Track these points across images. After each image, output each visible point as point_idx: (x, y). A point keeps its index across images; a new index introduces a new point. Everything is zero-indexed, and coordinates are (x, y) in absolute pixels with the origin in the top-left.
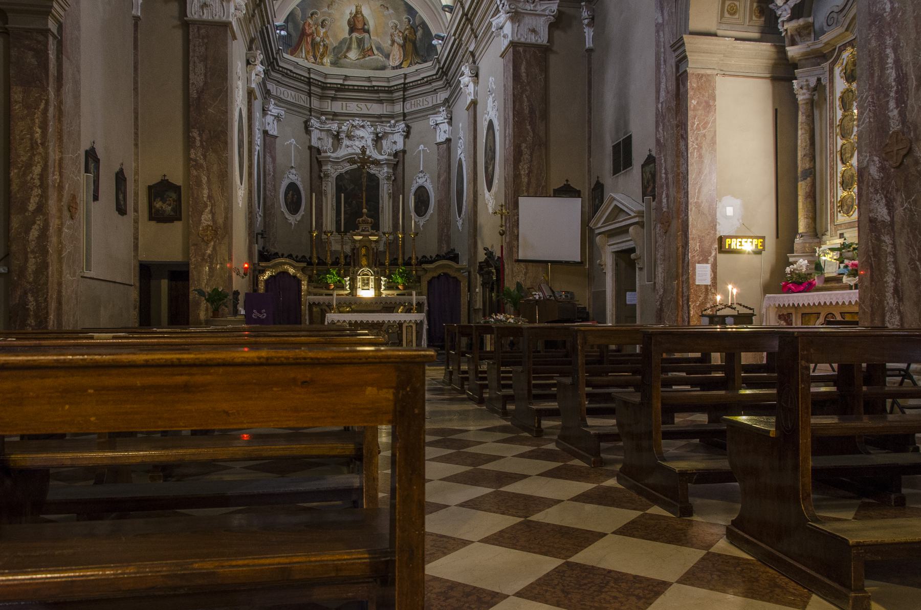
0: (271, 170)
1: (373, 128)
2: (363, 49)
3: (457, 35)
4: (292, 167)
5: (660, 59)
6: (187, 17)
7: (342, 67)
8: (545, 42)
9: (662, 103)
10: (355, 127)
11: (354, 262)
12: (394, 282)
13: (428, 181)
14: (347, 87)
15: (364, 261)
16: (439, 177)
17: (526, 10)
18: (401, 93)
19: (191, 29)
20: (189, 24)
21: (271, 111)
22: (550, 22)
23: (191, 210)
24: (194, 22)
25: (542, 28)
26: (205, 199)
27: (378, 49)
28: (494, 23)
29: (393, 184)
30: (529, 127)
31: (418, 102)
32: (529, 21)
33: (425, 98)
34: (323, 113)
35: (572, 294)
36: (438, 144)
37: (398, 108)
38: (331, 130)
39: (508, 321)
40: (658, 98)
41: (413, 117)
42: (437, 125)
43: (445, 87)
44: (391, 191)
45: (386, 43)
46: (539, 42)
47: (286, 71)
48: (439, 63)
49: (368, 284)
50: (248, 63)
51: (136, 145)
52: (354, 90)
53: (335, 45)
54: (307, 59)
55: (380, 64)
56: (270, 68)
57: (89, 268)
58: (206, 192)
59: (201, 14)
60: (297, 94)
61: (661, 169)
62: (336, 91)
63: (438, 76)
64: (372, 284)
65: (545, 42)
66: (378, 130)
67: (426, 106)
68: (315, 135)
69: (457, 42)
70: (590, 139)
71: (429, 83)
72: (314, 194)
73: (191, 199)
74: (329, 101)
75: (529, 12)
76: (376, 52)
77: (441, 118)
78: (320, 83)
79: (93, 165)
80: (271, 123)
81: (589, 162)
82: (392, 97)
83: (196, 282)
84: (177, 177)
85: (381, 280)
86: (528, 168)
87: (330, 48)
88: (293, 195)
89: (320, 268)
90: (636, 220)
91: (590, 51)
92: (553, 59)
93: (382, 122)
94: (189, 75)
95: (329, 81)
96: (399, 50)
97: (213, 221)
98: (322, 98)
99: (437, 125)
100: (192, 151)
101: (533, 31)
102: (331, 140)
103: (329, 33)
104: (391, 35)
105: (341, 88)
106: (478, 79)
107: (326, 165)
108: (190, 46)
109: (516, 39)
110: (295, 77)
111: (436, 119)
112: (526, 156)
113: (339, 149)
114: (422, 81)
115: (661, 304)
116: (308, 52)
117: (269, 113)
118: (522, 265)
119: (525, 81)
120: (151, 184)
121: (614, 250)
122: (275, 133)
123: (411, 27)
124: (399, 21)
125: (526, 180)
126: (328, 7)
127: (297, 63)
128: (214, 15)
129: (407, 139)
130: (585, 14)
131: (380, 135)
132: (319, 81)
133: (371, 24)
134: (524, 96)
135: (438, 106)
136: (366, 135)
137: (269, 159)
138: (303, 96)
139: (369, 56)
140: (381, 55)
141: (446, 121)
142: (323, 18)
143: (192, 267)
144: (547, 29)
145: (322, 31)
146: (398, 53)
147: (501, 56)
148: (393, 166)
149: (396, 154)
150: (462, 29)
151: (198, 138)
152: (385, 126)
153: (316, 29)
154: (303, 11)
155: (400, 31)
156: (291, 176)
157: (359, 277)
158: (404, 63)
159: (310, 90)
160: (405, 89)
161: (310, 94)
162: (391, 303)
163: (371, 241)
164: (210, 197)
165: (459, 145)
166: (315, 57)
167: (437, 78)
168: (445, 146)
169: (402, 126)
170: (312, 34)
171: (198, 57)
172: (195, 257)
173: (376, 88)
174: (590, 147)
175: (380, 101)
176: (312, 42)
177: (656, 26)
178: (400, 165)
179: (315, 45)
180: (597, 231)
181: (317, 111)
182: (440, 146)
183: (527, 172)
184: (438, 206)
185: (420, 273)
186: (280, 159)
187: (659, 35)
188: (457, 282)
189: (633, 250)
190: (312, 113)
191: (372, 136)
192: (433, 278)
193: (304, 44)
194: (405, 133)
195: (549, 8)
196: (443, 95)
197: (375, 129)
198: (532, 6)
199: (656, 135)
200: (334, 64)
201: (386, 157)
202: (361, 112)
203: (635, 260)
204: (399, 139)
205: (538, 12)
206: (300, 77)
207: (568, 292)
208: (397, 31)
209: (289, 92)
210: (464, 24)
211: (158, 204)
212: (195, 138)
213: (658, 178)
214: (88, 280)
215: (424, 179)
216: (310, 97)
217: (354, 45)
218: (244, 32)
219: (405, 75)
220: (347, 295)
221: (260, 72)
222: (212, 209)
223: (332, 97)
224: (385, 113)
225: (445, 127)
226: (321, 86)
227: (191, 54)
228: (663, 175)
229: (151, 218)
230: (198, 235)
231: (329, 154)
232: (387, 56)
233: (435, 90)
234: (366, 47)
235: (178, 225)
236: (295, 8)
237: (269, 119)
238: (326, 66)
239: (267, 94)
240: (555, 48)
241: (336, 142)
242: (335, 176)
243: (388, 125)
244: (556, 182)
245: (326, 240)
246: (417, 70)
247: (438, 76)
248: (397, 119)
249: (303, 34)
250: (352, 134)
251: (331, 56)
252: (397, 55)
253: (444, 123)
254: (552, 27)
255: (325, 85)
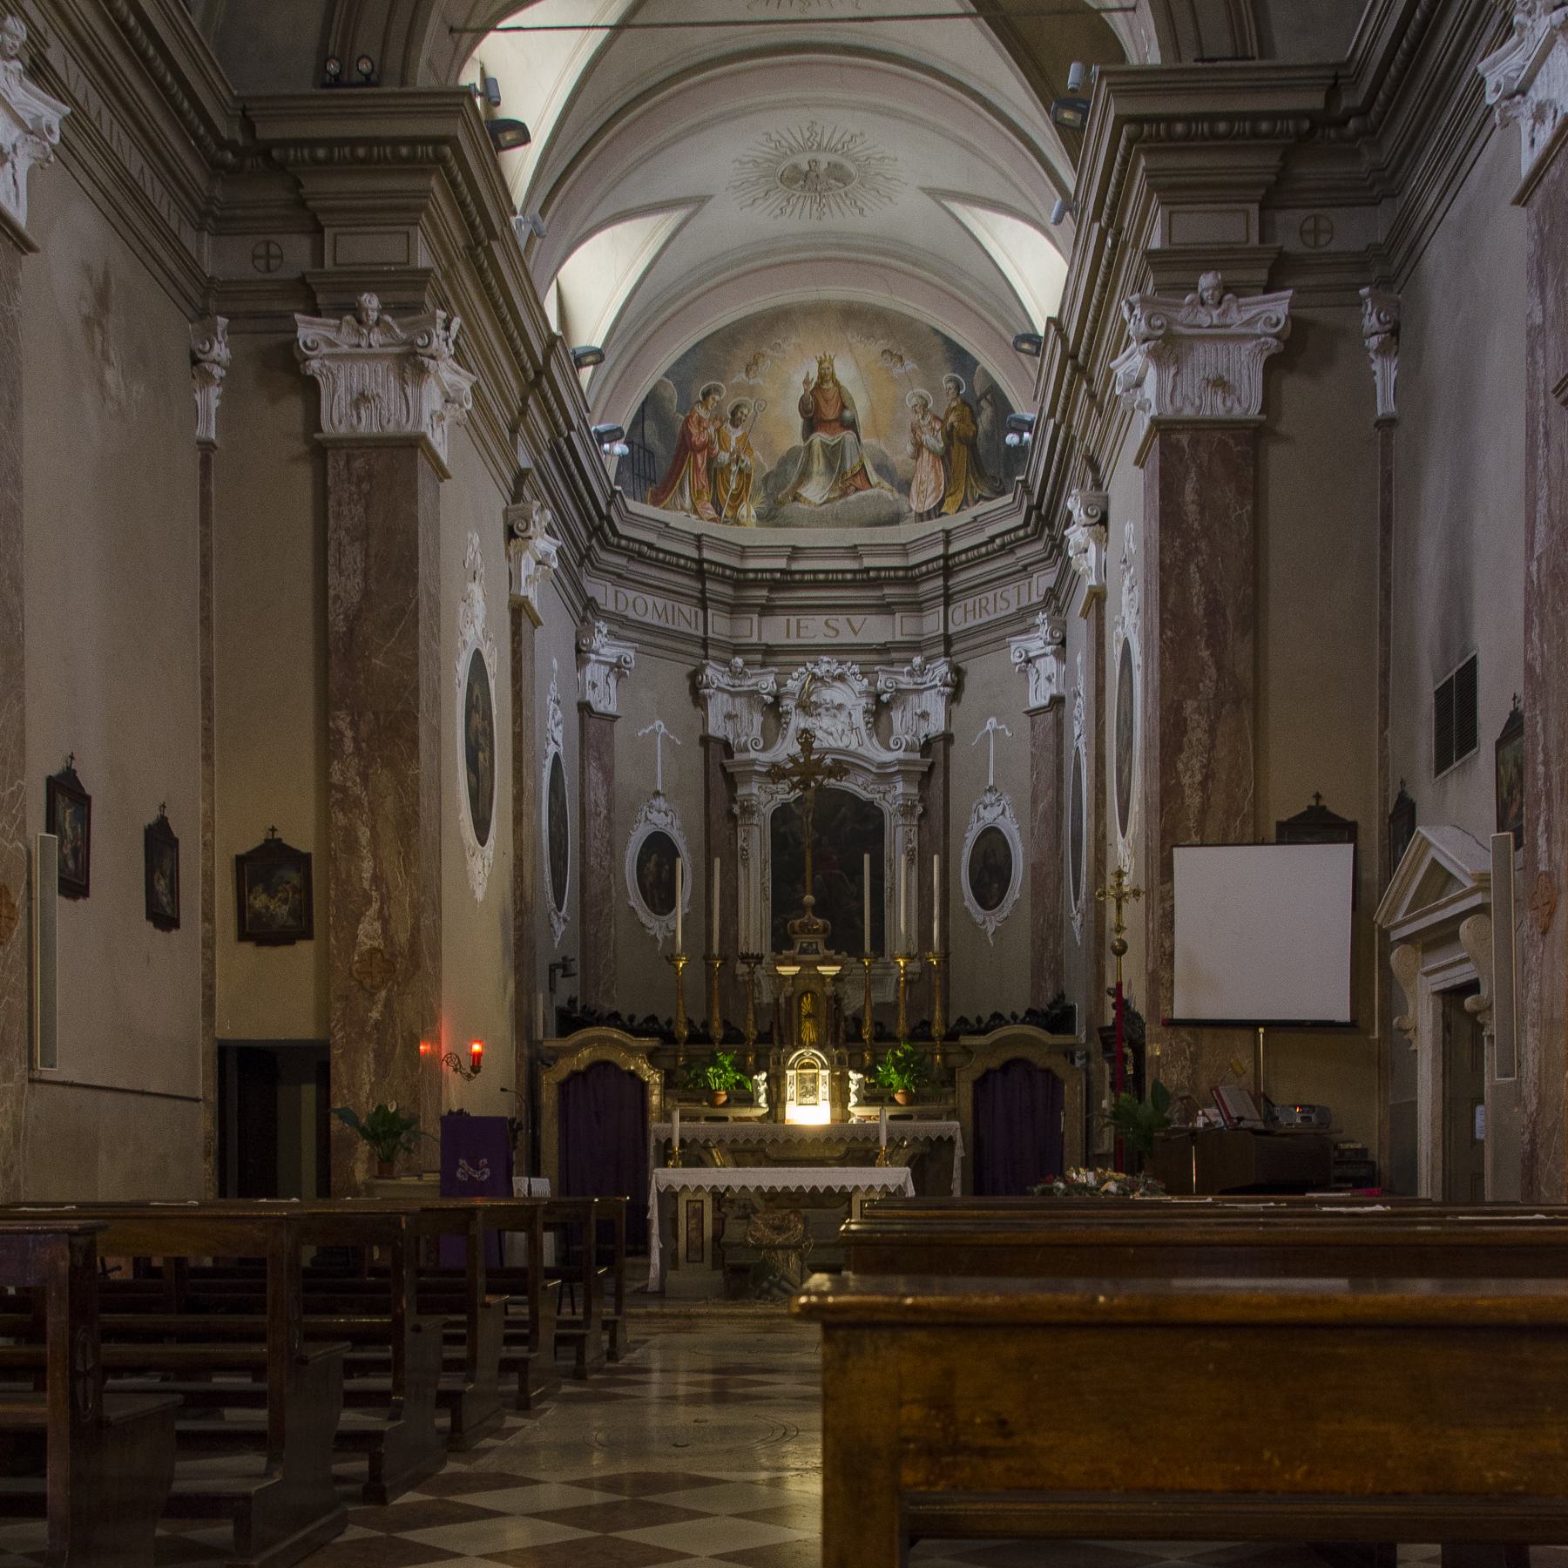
0: (602, 801)
1: (866, 681)
2: (842, 473)
3: (1058, 415)
4: (657, 794)
5: (1535, 431)
6: (320, 430)
7: (786, 526)
8: (1254, 411)
9: (1539, 559)
10: (821, 679)
11: (781, 1036)
12: (882, 1085)
13: (1007, 813)
14: (797, 577)
15: (809, 1031)
16: (1034, 801)
17: (1200, 327)
18: (940, 582)
19: (330, 462)
20: (325, 450)
21: (597, 653)
22: (1266, 354)
23: (333, 910)
24: (338, 443)
25: (1245, 372)
26: (366, 885)
27: (881, 469)
28: (1120, 373)
29: (919, 827)
30: (1205, 654)
31: (984, 603)
32: (1206, 358)
33: (999, 591)
34: (738, 650)
35: (1323, 1112)
36: (1033, 713)
37: (932, 623)
38: (757, 692)
39: (1103, 1189)
40: (1530, 545)
41: (971, 643)
42: (1029, 661)
43: (1049, 557)
44: (915, 844)
45: (900, 453)
46: (1237, 412)
47: (637, 546)
48: (1030, 493)
49: (814, 1091)
50: (511, 534)
51: (208, 758)
52: (816, 585)
53: (768, 470)
54: (696, 512)
55: (885, 511)
56: (594, 541)
57: (49, 1061)
58: (367, 866)
59: (355, 421)
60: (669, 603)
61: (1534, 753)
62: (771, 590)
63: (1029, 530)
64: (824, 1090)
65: (1254, 411)
66: (880, 685)
67: (1003, 613)
68: (718, 706)
69: (1062, 434)
70: (1385, 675)
71: (1007, 549)
72: (717, 862)
73: (333, 886)
74: (755, 617)
75: (1210, 331)
76: (874, 478)
77: (1037, 642)
78: (728, 572)
79: (69, 811)
80: (601, 683)
81: (1384, 741)
82: (916, 595)
83: (345, 1091)
84: (301, 837)
85: (849, 1079)
86: (1204, 766)
87: (756, 478)
88: (659, 865)
89: (697, 1049)
90: (1476, 900)
91: (1388, 423)
92: (1277, 455)
93: (891, 663)
94: (326, 575)
95: (914, 560)
96: (934, 466)
97: (385, 939)
98: (736, 609)
99: (1029, 661)
100: (336, 765)
101: (1220, 384)
102: (758, 719)
103: (751, 440)
104: (914, 431)
105: (784, 581)
106: (1106, 530)
107: (748, 782)
108: (331, 503)
109: (1169, 412)
110: (663, 561)
111: (1029, 645)
112: (1197, 735)
113: (780, 740)
114: (990, 547)
115: (1532, 1141)
116: (700, 492)
117: (593, 657)
118: (1184, 1033)
119: (1196, 525)
120: (242, 852)
121: (1437, 988)
122: (612, 709)
123: (964, 403)
124: (932, 389)
125: (1198, 800)
126: (747, 371)
127: (667, 525)
128: (384, 423)
129: (955, 705)
130: (1371, 322)
131: (885, 698)
132: (725, 566)
133: (861, 406)
134: (1193, 568)
135: (1032, 610)
136: (849, 696)
137: (594, 775)
138: (685, 609)
139: (857, 490)
140: (887, 485)
141: (1049, 649)
142: (736, 401)
143: (336, 1052)
144: (1260, 375)
145: (735, 435)
146: (932, 476)
147: (1136, 463)
148: (919, 777)
149: (927, 747)
150: (1067, 397)
151: (349, 733)
152: (896, 673)
153: (718, 431)
154: (683, 386)
155: (936, 418)
156: (653, 816)
157: (790, 1073)
158: (949, 500)
159: (703, 591)
160: (948, 572)
161: (703, 603)
162: (854, 1139)
163: (823, 977)
164: (377, 879)
165: (1076, 712)
166: (717, 504)
167: (1027, 536)
168: (1050, 716)
169: (941, 669)
170: (708, 446)
171: (347, 530)
172: (342, 1028)
173: (872, 574)
174: (1384, 698)
175: (886, 608)
176: (708, 469)
177: (1528, 335)
178: (939, 771)
179: (715, 473)
180: (1395, 935)
181: (720, 645)
182: (1038, 718)
183: (1199, 778)
184: (1033, 878)
185: (954, 1060)
186: (625, 773)
187: (1534, 362)
188: (1054, 1083)
189: (1472, 987)
190: (711, 652)
191: (863, 701)
192: (989, 1072)
193: (687, 471)
194: (948, 690)
195: (1264, 316)
196: (1045, 580)
197: (873, 683)
198: (1215, 313)
199: (1526, 651)
200: (768, 518)
201: (900, 754)
202: (835, 641)
203: (1476, 1013)
204: (934, 704)
205: (1232, 330)
206: (675, 560)
207: (1312, 1108)
208: (929, 417)
209: (649, 599)
210: (1071, 383)
211: (259, 901)
212: (342, 734)
213: (1528, 777)
214: (60, 1088)
215: (1000, 810)
216: (705, 609)
217: (818, 465)
218: (495, 463)
219: (947, 533)
220: (760, 1119)
221: (547, 554)
222: (381, 909)
223: (762, 606)
224: (899, 638)
225: (1048, 665)
226: (729, 578)
227: (331, 522)
228: (1541, 769)
229: (243, 936)
230: (351, 974)
231: (753, 755)
232: (904, 487)
233: (1025, 568)
234: (848, 466)
235: (305, 948)
236: (660, 382)
237: (594, 672)
238: (748, 527)
239: (587, 611)
240: (1282, 428)
241: (772, 722)
242: (768, 811)
243: (906, 670)
244: (1287, 804)
245: (747, 978)
246: (975, 518)
247: (1029, 530)
248: (927, 653)
249: (685, 448)
250: (813, 698)
251: (759, 499)
252: (928, 482)
253: (1045, 655)
254: (1274, 367)
255: (742, 576)
